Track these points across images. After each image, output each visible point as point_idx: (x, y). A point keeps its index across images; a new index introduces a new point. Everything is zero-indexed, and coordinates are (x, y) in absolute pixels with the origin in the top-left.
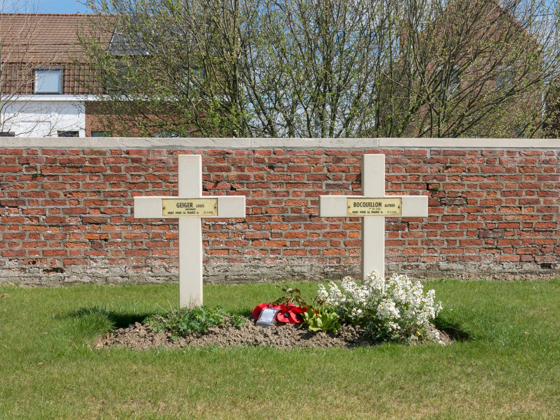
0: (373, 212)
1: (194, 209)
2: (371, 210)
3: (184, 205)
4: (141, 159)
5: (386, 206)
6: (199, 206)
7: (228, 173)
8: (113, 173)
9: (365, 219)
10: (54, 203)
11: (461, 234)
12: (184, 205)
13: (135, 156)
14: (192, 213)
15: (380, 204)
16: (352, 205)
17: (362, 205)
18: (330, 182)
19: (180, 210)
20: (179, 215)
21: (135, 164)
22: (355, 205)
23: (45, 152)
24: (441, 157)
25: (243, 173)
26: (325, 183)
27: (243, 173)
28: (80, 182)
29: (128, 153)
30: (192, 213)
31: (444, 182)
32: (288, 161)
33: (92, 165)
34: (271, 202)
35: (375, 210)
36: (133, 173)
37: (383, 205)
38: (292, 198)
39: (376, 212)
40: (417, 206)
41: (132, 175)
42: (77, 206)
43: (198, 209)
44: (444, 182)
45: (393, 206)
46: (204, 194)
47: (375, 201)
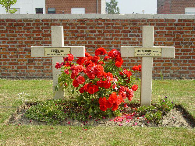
0: (147, 55)
1: (59, 53)
2: (146, 54)
3: (54, 51)
4: (48, 23)
5: (153, 52)
6: (61, 51)
7: (86, 30)
8: (37, 30)
9: (143, 59)
10: (13, 42)
11: (190, 57)
12: (54, 51)
13: (46, 22)
14: (59, 54)
15: (151, 51)
16: (137, 51)
17: (142, 51)
18: (131, 34)
19: (52, 53)
20: (52, 55)
21: (46, 26)
22: (138, 51)
23: (7, 20)
24: (182, 22)
25: (93, 30)
26: (129, 34)
27: (93, 30)
28: (23, 34)
29: (42, 21)
30: (59, 54)
31: (183, 34)
32: (112, 24)
33: (27, 26)
34: (105, 42)
35: (148, 54)
36: (45, 30)
37: (152, 51)
38: (114, 41)
39: (149, 55)
40: (169, 52)
41: (44, 31)
42: (22, 44)
43: (61, 53)
44: (183, 34)
45: (157, 52)
46: (64, 45)
47: (148, 49)
